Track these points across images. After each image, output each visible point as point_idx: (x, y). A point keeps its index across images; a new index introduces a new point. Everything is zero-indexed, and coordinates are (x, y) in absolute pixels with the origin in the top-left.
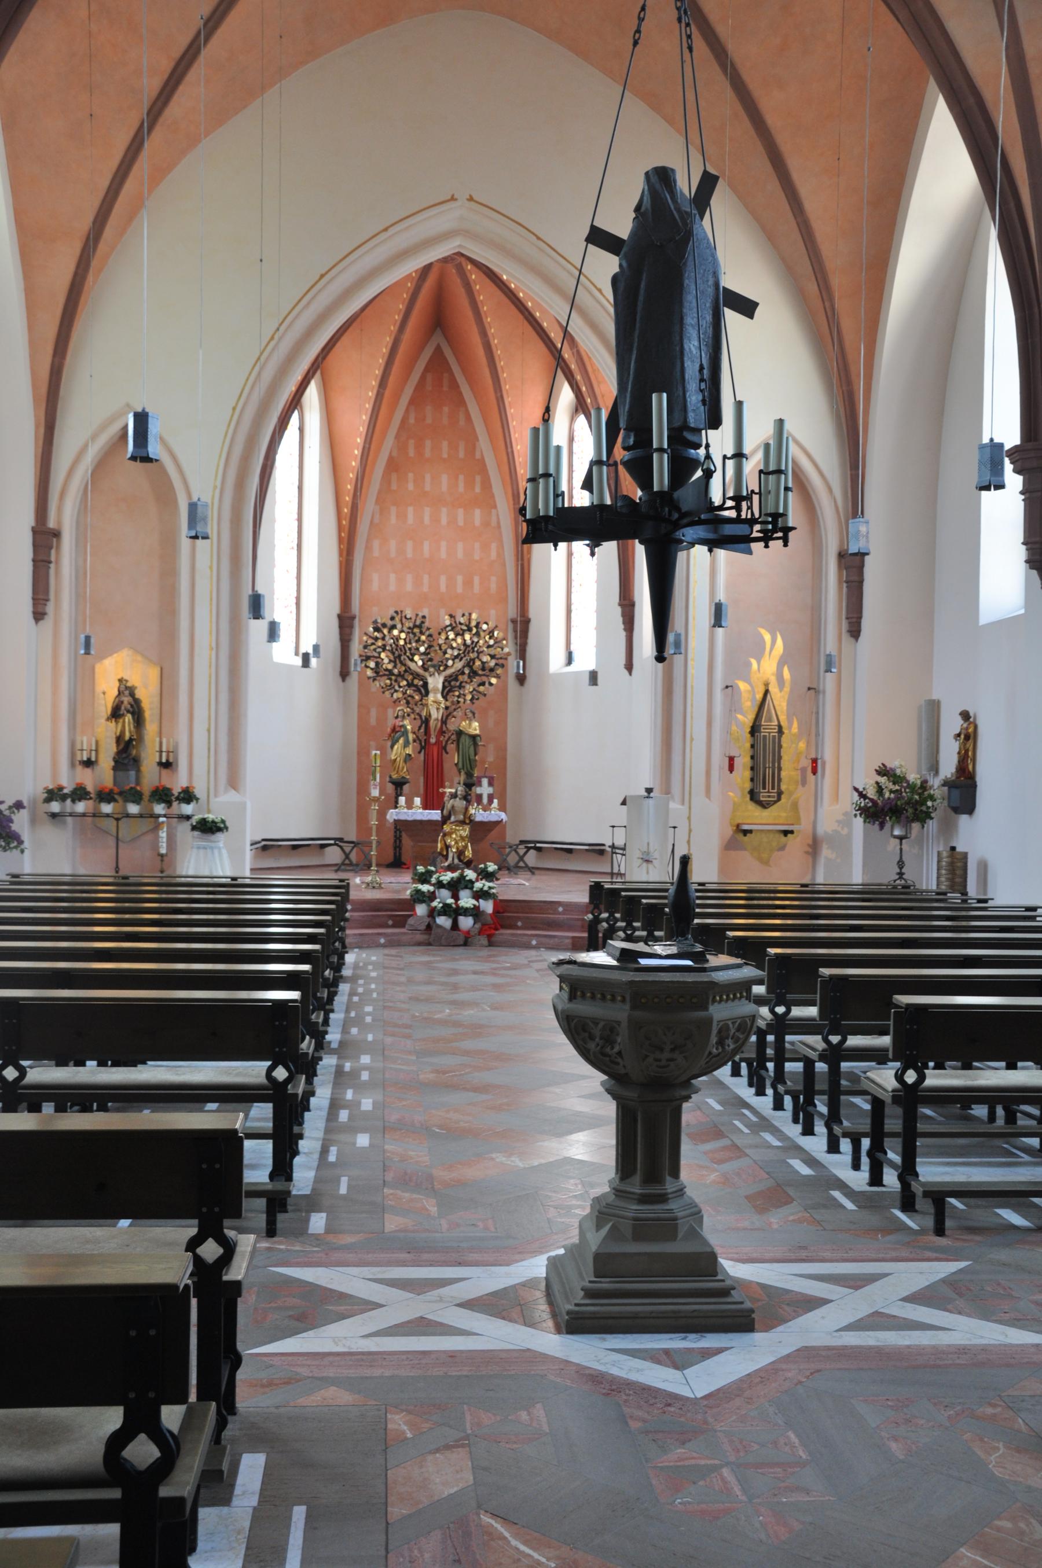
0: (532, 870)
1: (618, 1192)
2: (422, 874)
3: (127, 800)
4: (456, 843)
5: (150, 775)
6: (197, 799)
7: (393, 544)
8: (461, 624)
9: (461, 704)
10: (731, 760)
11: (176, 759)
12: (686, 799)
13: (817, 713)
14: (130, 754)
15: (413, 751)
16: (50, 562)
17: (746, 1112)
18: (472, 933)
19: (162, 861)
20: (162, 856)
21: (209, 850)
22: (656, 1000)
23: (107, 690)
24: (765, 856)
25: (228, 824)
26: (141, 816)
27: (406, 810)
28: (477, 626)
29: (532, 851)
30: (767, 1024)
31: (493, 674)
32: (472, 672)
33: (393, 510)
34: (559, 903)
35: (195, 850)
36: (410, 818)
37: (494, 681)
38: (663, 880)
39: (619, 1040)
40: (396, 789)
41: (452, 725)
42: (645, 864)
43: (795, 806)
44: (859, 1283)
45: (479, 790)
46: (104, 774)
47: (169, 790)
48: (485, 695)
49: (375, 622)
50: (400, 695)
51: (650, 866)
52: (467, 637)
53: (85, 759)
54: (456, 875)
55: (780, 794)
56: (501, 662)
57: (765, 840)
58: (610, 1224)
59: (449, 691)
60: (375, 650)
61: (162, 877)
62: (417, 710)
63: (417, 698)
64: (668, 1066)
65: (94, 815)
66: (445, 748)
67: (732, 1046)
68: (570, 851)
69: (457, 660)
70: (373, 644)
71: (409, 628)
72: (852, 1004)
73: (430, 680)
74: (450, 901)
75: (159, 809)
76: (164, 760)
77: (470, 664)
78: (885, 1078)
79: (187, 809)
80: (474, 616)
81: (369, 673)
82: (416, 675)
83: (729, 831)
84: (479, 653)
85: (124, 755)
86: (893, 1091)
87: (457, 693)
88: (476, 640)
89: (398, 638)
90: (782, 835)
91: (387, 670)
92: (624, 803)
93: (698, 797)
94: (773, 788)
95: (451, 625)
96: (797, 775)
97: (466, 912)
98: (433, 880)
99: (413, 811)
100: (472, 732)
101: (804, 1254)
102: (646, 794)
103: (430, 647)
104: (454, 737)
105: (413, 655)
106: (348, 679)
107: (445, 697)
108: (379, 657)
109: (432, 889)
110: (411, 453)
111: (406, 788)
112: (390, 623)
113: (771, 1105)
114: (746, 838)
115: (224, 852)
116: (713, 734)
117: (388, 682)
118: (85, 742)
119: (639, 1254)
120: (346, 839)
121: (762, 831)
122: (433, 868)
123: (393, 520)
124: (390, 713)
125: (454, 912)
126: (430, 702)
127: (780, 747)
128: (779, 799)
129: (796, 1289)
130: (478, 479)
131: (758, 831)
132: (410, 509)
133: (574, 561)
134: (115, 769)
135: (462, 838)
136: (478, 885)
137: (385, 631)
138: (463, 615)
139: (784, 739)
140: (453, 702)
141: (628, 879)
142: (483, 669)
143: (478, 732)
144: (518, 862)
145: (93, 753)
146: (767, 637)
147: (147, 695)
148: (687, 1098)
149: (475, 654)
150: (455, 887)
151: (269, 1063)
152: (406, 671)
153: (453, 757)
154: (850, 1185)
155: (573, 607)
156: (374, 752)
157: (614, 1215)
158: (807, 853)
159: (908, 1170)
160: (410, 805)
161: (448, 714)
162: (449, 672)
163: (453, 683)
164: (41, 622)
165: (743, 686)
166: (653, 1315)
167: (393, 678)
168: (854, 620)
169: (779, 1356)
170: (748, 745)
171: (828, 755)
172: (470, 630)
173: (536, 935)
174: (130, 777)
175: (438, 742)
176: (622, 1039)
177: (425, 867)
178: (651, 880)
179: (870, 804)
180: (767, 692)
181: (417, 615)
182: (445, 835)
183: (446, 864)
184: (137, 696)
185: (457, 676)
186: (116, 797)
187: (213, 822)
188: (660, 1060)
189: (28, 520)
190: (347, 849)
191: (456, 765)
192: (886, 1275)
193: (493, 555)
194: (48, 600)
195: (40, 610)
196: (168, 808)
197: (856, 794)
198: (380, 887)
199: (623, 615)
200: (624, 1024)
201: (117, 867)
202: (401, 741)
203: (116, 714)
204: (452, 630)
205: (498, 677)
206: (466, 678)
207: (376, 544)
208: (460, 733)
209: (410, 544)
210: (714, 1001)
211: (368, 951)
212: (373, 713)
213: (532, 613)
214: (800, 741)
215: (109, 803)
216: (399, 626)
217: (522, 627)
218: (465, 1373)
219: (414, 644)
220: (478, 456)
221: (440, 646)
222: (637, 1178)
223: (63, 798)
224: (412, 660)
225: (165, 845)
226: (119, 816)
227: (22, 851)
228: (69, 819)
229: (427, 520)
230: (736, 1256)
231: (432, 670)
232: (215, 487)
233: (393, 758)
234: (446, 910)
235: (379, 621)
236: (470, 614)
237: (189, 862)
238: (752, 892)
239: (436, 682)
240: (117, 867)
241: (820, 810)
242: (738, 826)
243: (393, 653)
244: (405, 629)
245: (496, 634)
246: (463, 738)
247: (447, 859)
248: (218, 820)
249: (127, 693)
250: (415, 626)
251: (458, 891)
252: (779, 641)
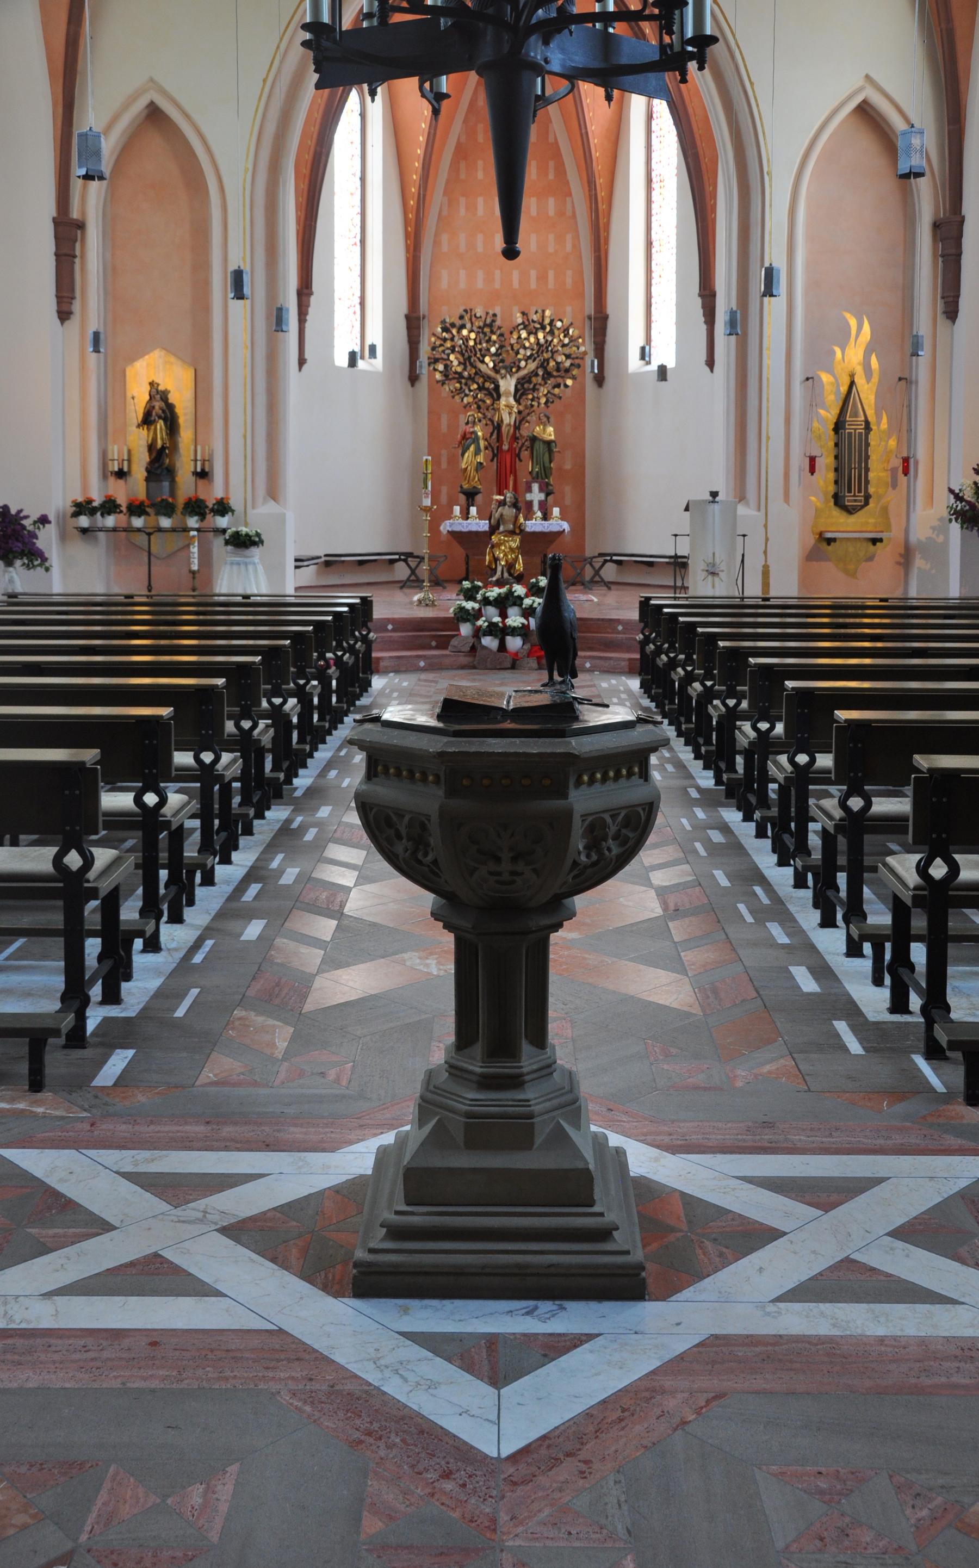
0: (608, 585)
1: (453, 1069)
2: (468, 589)
3: (158, 513)
4: (505, 555)
5: (186, 485)
6: (233, 511)
7: (462, 239)
8: (533, 321)
9: (535, 408)
10: (812, 460)
11: (211, 467)
12: (762, 505)
13: (909, 406)
14: (163, 463)
15: (485, 458)
16: (75, 257)
17: (758, 890)
18: (520, 655)
19: (194, 578)
20: (193, 573)
21: (242, 567)
22: (485, 782)
23: (139, 396)
24: (851, 567)
25: (263, 537)
26: (173, 530)
27: (461, 521)
28: (551, 323)
29: (609, 565)
30: (786, 778)
31: (569, 375)
32: (547, 372)
33: (462, 200)
34: (618, 621)
35: (228, 567)
36: (465, 530)
37: (569, 382)
38: (731, 594)
39: (432, 841)
40: (468, 500)
41: (525, 432)
42: (710, 577)
43: (885, 511)
44: (834, 1197)
45: (528, 497)
46: (138, 485)
47: (203, 501)
48: (560, 398)
49: (443, 322)
50: (471, 400)
51: (716, 579)
52: (541, 335)
53: (116, 469)
54: (503, 590)
55: (867, 498)
56: (577, 361)
57: (851, 549)
58: (437, 1118)
60: (443, 352)
61: (193, 596)
62: (489, 415)
63: (488, 402)
64: (513, 882)
65: (125, 530)
66: (518, 455)
67: (616, 851)
68: (651, 564)
69: (530, 361)
70: (441, 345)
71: (479, 327)
72: (871, 757)
73: (502, 383)
74: (497, 619)
75: (193, 522)
76: (199, 470)
77: (544, 365)
78: (905, 866)
79: (222, 522)
80: (548, 313)
81: (438, 376)
82: (487, 378)
83: (811, 540)
84: (553, 352)
85: (157, 465)
86: (916, 888)
87: (530, 396)
88: (550, 339)
89: (467, 339)
90: (870, 544)
91: (456, 373)
92: (687, 509)
93: (776, 503)
94: (860, 491)
95: (523, 323)
96: (886, 476)
97: (514, 631)
98: (479, 597)
99: (469, 521)
101: (767, 1137)
102: (711, 498)
103: (501, 347)
104: (527, 444)
105: (484, 356)
106: (417, 384)
107: (517, 401)
108: (448, 359)
109: (476, 606)
111: (479, 498)
112: (458, 323)
113: (791, 881)
114: (830, 548)
115: (260, 568)
116: (792, 431)
117: (458, 385)
118: (114, 451)
119: (474, 1170)
120: (415, 554)
121: (848, 539)
122: (480, 584)
123: (462, 211)
124: (462, 419)
125: (501, 632)
126: (502, 407)
127: (867, 445)
128: (867, 503)
129: (736, 1208)
131: (840, 539)
133: (654, 251)
134: (147, 480)
135: (512, 549)
136: (527, 602)
137: (454, 331)
138: (536, 312)
139: (872, 436)
140: (526, 407)
141: (691, 593)
142: (558, 370)
143: (553, 437)
144: (594, 577)
145: (126, 463)
146: (853, 322)
147: (182, 399)
148: (558, 926)
149: (550, 354)
150: (502, 604)
151: (54, 850)
152: (476, 373)
153: (527, 466)
154: (864, 1010)
155: (653, 300)
156: (425, 458)
157: (441, 1106)
158: (898, 563)
159: (936, 1001)
160: (466, 515)
161: (522, 418)
162: (522, 373)
163: (526, 386)
164: (67, 323)
165: (825, 378)
166: (488, 1270)
167: (463, 381)
168: (951, 299)
169: (668, 1356)
170: (831, 444)
171: (921, 453)
172: (543, 328)
173: (590, 657)
174: (163, 488)
175: (511, 449)
176: (435, 838)
177: (472, 582)
178: (717, 594)
179: (967, 507)
180: (852, 383)
181: (487, 313)
182: (493, 547)
183: (494, 579)
184: (170, 401)
185: (530, 378)
186: (148, 510)
187: (247, 535)
188: (499, 874)
189: (49, 209)
190: (413, 565)
191: (530, 473)
192: (879, 1181)
193: (569, 247)
194: (73, 298)
195: (65, 308)
196: (202, 521)
197: (952, 496)
198: (433, 605)
199: (704, 306)
200: (435, 818)
201: (150, 585)
202: (472, 448)
203: (147, 420)
204: (524, 328)
205: (574, 378)
206: (540, 380)
207: (445, 238)
208: (534, 439)
209: (480, 237)
210: (579, 783)
211: (403, 676)
213: (611, 309)
214: (889, 438)
215: (140, 516)
216: (469, 325)
217: (600, 324)
218: (154, 1384)
219: (484, 345)
220: (551, 140)
221: (512, 346)
222: (478, 1049)
223: (92, 512)
224: (483, 362)
225: (196, 561)
226: (150, 531)
227: (47, 569)
228: (101, 535)
230: (667, 1139)
231: (503, 371)
232: (246, 170)
233: (464, 466)
234: (492, 630)
235: (448, 320)
236: (543, 311)
237: (222, 579)
238: (839, 608)
239: (508, 384)
240: (150, 585)
241: (912, 516)
242: (821, 534)
243: (463, 355)
244: (475, 328)
245: (571, 331)
246: (537, 445)
247: (495, 573)
248: (252, 533)
249: (158, 397)
250: (485, 325)
251: (506, 608)
252: (866, 327)
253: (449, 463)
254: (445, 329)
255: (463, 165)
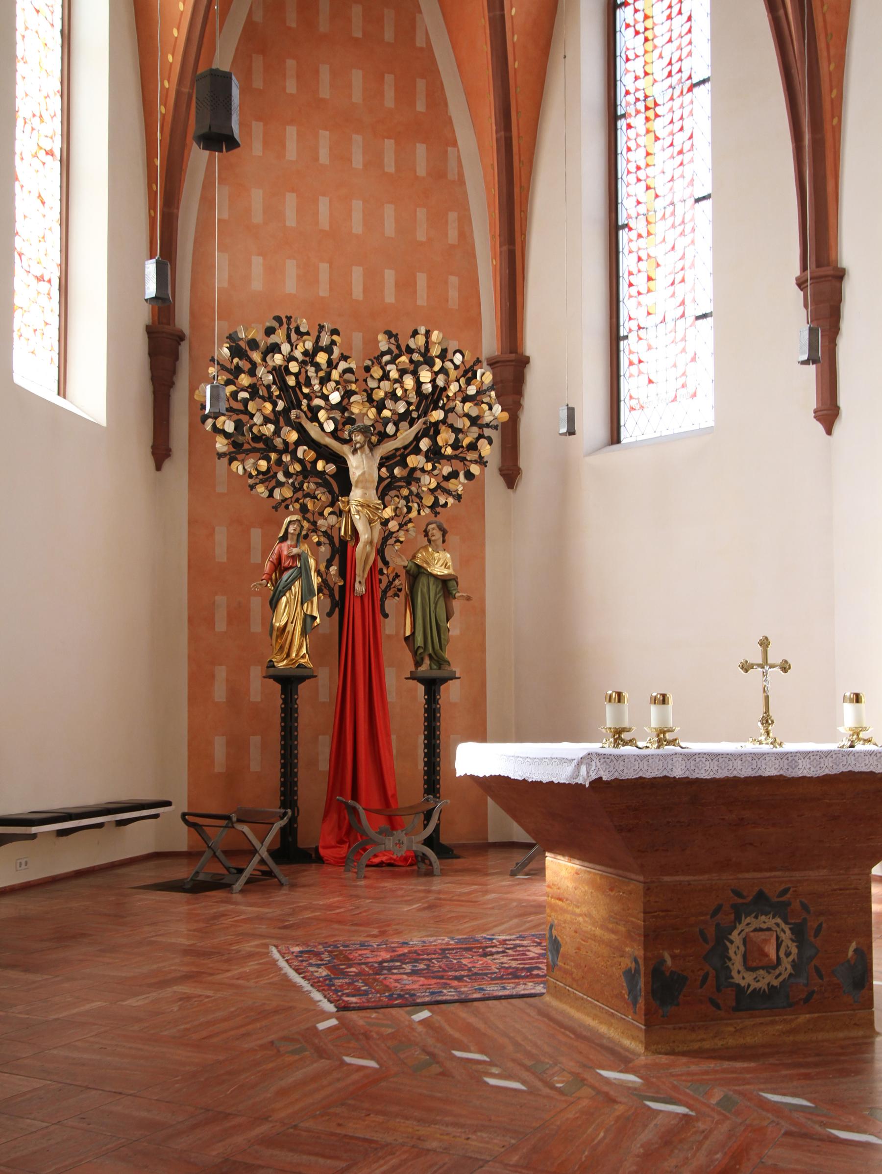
7: (257, 197)
28: (443, 355)
50: (288, 493)
59: (389, 488)
69: (404, 425)
80: (435, 336)
81: (221, 444)
91: (257, 438)
100: (439, 570)
106: (167, 465)
110: (292, 19)
112: (264, 342)
117: (263, 465)
130: (421, 85)
132: (291, 132)
153: (397, 622)
162: (388, 447)
172: (430, 363)
193: (453, 235)
202: (296, 587)
207: (220, 194)
208: (416, 574)
209: (291, 200)
212: (221, 537)
220: (420, 42)
224: (314, 418)
229: (324, 156)
235: (242, 335)
236: (428, 334)
239: (360, 465)
244: (298, 354)
246: (423, 580)
250: (317, 349)
253: (230, 622)
254: (236, 351)
255: (258, 62)
